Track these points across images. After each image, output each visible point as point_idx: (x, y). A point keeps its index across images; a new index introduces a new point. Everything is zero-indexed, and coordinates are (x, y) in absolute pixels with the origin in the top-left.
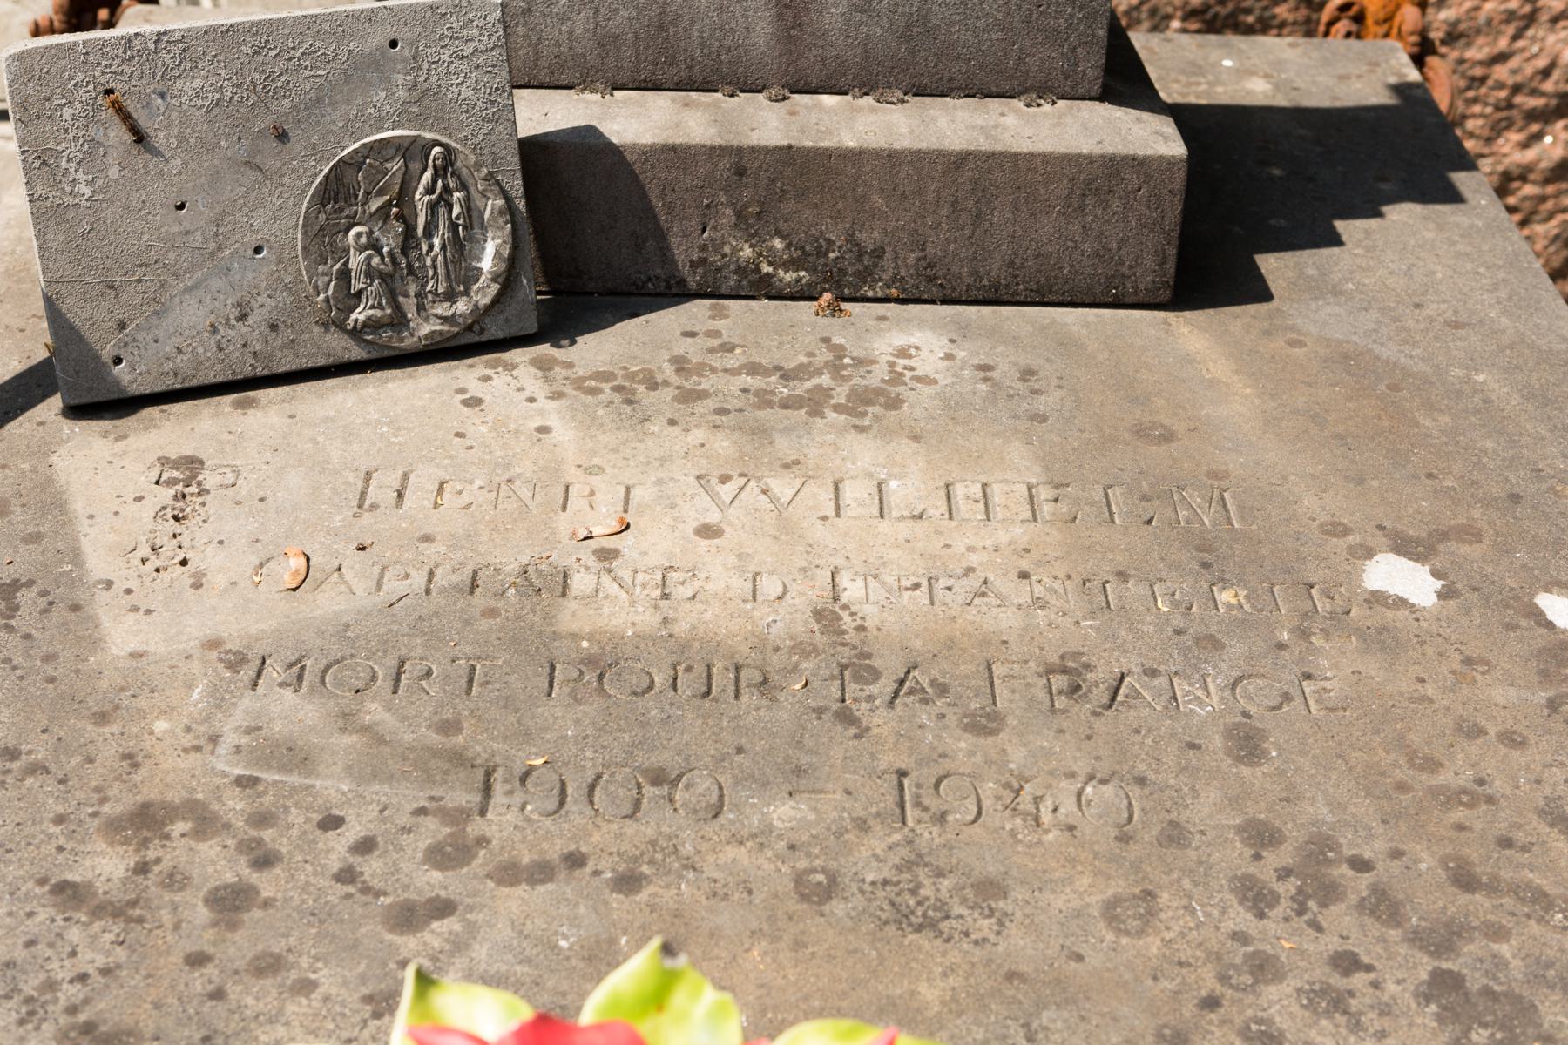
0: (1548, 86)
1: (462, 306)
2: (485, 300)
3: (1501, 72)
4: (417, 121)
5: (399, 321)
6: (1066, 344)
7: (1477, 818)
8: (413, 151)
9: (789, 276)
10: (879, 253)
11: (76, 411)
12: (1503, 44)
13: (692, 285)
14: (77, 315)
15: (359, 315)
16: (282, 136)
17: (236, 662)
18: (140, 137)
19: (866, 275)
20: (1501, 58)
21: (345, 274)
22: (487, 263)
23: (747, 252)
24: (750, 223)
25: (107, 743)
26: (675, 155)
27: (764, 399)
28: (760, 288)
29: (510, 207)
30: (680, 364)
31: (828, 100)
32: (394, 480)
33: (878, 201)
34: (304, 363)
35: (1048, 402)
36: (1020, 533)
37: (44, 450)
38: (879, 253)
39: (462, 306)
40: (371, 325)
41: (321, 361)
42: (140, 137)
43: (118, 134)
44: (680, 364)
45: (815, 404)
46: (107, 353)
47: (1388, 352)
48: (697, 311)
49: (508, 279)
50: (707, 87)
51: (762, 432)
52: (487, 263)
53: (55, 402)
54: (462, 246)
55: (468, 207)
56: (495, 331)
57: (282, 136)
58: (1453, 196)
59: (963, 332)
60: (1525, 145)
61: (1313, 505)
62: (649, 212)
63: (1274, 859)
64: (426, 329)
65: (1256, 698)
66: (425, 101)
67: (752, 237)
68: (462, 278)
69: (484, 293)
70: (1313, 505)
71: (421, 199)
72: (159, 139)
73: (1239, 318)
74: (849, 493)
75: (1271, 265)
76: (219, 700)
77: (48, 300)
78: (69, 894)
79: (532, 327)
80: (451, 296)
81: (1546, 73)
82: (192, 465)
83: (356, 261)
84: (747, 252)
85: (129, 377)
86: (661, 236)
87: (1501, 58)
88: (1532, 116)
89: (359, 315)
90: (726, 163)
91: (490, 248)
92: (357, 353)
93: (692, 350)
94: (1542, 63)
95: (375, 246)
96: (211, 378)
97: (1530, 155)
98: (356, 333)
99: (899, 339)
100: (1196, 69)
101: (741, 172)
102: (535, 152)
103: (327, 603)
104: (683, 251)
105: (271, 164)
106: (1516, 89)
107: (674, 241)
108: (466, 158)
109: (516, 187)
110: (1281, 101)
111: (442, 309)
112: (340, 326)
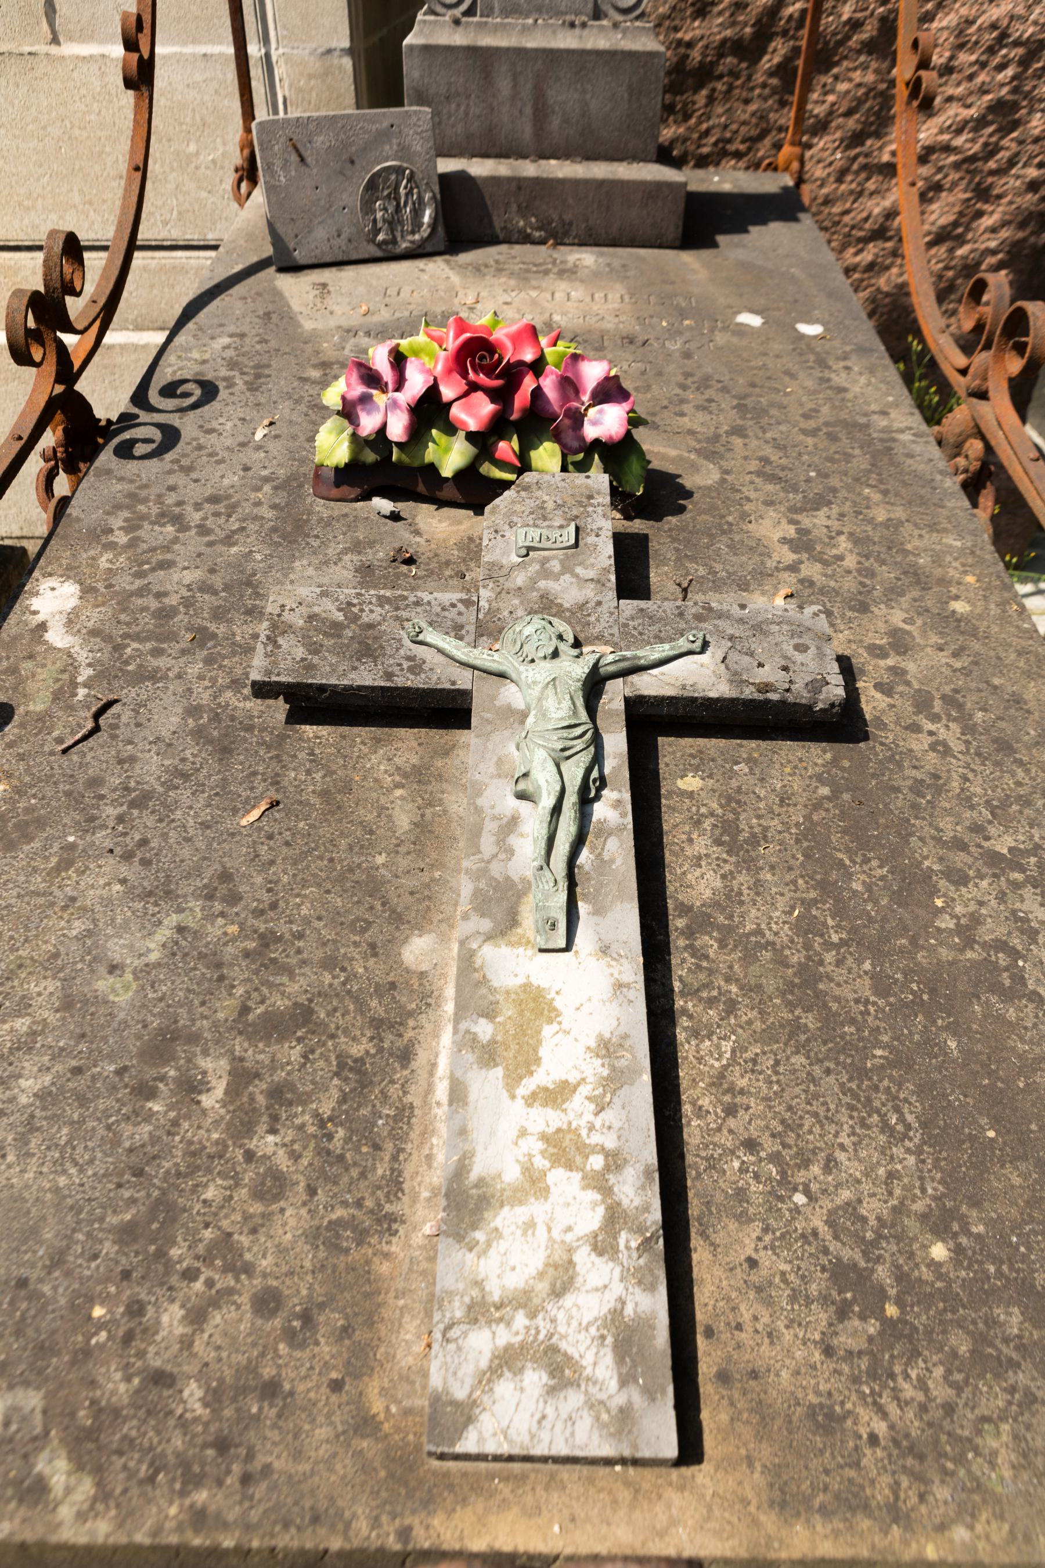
0: (867, 226)
1: (417, 237)
2: (425, 235)
3: (847, 219)
4: (400, 159)
5: (394, 242)
6: (639, 259)
7: (761, 373)
8: (399, 171)
9: (537, 234)
10: (571, 224)
11: (282, 270)
12: (848, 205)
13: (501, 237)
14: (281, 230)
15: (381, 237)
16: (352, 162)
17: (348, 331)
18: (302, 159)
19: (566, 234)
20: (847, 212)
21: (375, 221)
22: (426, 219)
23: (521, 223)
24: (524, 211)
25: (309, 348)
26: (495, 181)
27: (528, 271)
28: (526, 239)
29: (434, 197)
30: (497, 262)
31: (553, 162)
32: (395, 290)
33: (571, 201)
34: (361, 256)
35: (631, 273)
36: (616, 306)
37: (272, 280)
38: (571, 224)
39: (417, 237)
40: (385, 242)
41: (366, 256)
42: (302, 159)
43: (294, 157)
44: (497, 262)
45: (546, 272)
46: (291, 246)
47: (760, 263)
48: (504, 248)
49: (433, 226)
50: (507, 156)
51: (527, 279)
52: (426, 219)
53: (273, 269)
54: (417, 213)
55: (420, 198)
56: (429, 249)
57: (352, 162)
58: (796, 220)
59: (602, 254)
60: (856, 254)
61: (722, 301)
62: (485, 206)
63: (690, 380)
64: (404, 245)
65: (692, 346)
66: (403, 151)
67: (524, 217)
68: (417, 225)
69: (425, 231)
70: (722, 301)
71: (402, 191)
72: (309, 160)
73: (706, 254)
74: (557, 295)
75: (721, 239)
76: (343, 339)
77: (271, 226)
78: (304, 380)
79: (442, 248)
80: (413, 232)
81: (866, 219)
82: (324, 285)
83: (379, 215)
84: (521, 223)
85: (300, 256)
86: (489, 216)
87: (847, 212)
88: (860, 240)
89: (381, 237)
90: (514, 185)
91: (428, 213)
92: (379, 254)
93: (501, 258)
94: (864, 214)
95: (385, 209)
96: (328, 259)
97: (858, 259)
98: (379, 245)
99: (577, 256)
100: (703, 181)
101: (519, 188)
102: (445, 179)
103: (376, 319)
104: (498, 223)
105: (349, 173)
106: (853, 227)
107: (495, 218)
108: (419, 175)
109: (436, 188)
110: (736, 190)
111: (410, 238)
112: (373, 241)
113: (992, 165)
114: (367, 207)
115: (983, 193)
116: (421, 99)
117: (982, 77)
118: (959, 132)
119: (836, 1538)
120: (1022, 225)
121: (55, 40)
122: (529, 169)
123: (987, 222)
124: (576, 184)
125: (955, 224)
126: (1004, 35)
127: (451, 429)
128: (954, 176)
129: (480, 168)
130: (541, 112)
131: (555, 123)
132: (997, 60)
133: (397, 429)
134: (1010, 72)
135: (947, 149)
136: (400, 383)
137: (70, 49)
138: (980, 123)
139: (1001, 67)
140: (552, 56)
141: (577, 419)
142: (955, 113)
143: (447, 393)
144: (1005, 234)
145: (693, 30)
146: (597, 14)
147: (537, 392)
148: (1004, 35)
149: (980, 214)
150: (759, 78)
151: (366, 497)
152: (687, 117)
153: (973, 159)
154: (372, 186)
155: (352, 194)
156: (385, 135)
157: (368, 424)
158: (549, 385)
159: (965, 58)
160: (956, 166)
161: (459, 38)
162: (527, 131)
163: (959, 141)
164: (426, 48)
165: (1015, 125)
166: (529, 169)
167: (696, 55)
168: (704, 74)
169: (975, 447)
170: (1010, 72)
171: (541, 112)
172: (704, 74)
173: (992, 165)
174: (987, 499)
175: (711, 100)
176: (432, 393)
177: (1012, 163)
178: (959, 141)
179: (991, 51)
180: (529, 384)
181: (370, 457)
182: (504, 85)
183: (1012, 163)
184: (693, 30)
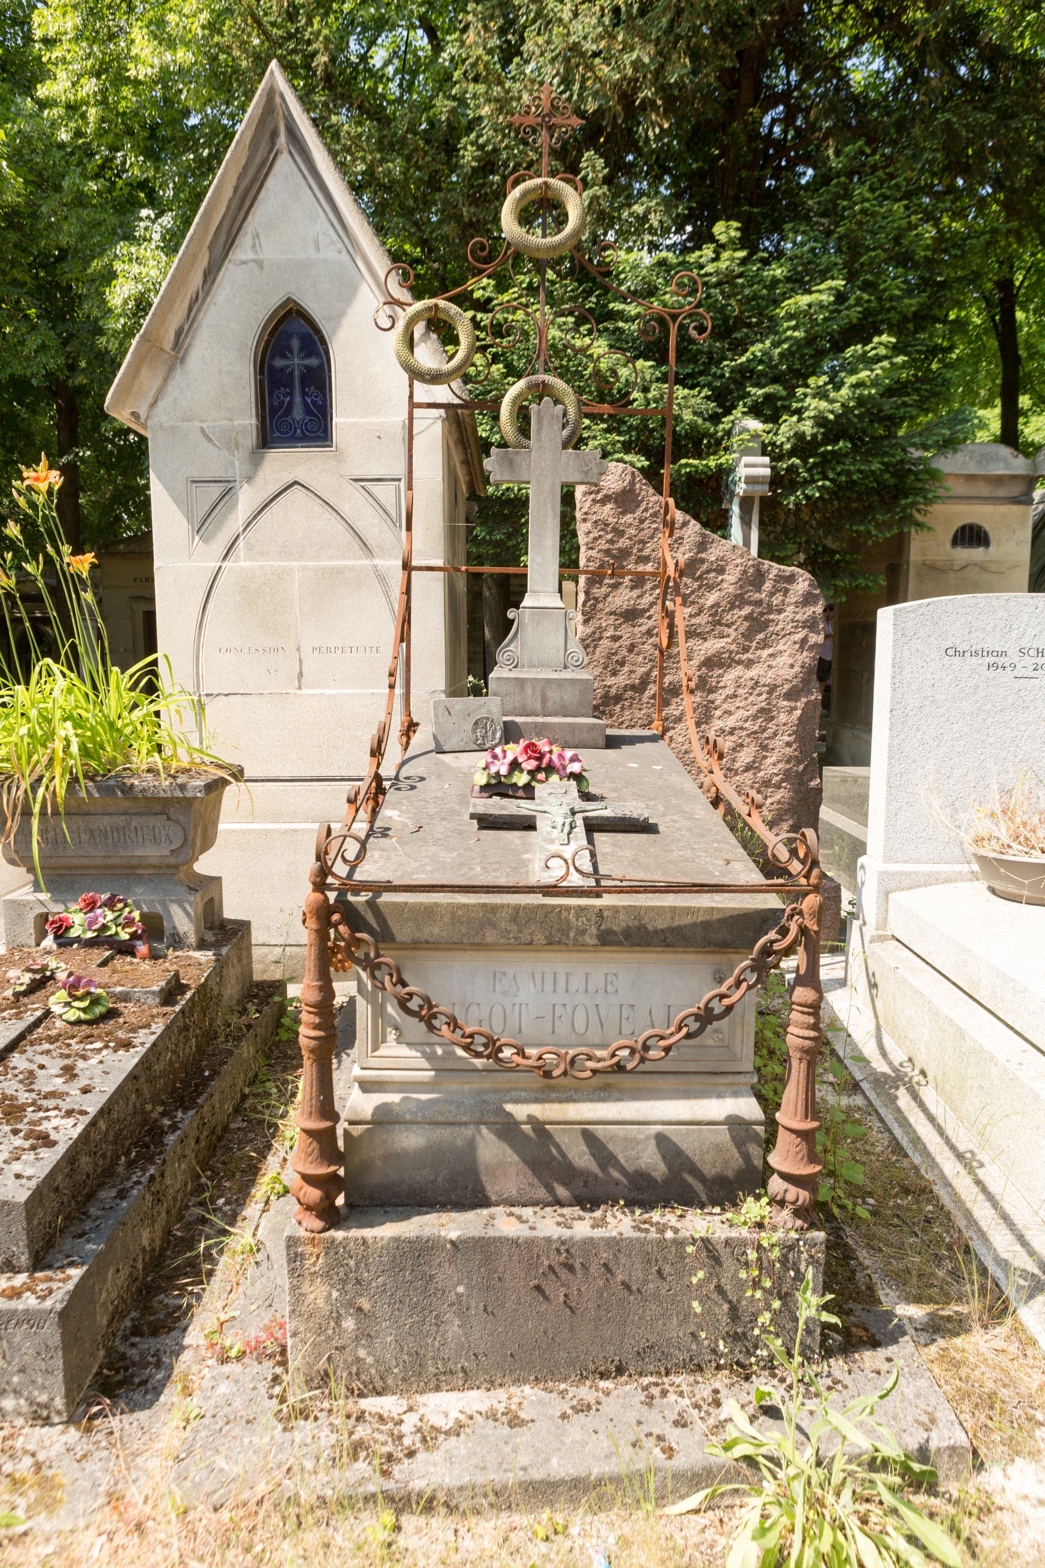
26: (526, 723)
54: (494, 733)
68: (494, 738)
113: (765, 735)
114: (474, 731)
115: (764, 748)
116: (495, 694)
117: (751, 699)
118: (746, 721)
119: (446, 73)
120: (788, 762)
121: (300, 688)
122: (540, 719)
123: (769, 761)
124: (559, 724)
125: (754, 762)
126: (757, 683)
127: (522, 771)
128: (748, 740)
129: (519, 719)
130: (544, 700)
131: (550, 704)
132: (756, 692)
133: (504, 771)
134: (764, 696)
135: (742, 728)
136: (505, 757)
137: (305, 691)
138: (755, 717)
139: (760, 695)
140: (549, 681)
141: (564, 768)
142: (742, 713)
143: (520, 760)
144: (780, 766)
145: (610, 681)
146: (566, 667)
147: (551, 760)
148: (757, 683)
149: (765, 757)
150: (645, 699)
151: (490, 797)
152: (611, 716)
153: (755, 732)
154: (476, 723)
155: (469, 726)
156: (481, 706)
157: (493, 770)
158: (555, 757)
159: (740, 691)
160: (748, 736)
161: (511, 675)
162: (538, 706)
163: (747, 725)
164: (499, 678)
165: (773, 718)
166: (540, 719)
167: (613, 691)
168: (618, 699)
169: (714, 789)
170: (764, 696)
171: (544, 700)
172: (618, 699)
173: (765, 735)
174: (722, 808)
175: (623, 709)
176: (516, 759)
177: (775, 734)
178: (747, 725)
179: (752, 688)
180: (548, 756)
181: (493, 781)
182: (529, 690)
183: (775, 734)
184: (610, 681)
